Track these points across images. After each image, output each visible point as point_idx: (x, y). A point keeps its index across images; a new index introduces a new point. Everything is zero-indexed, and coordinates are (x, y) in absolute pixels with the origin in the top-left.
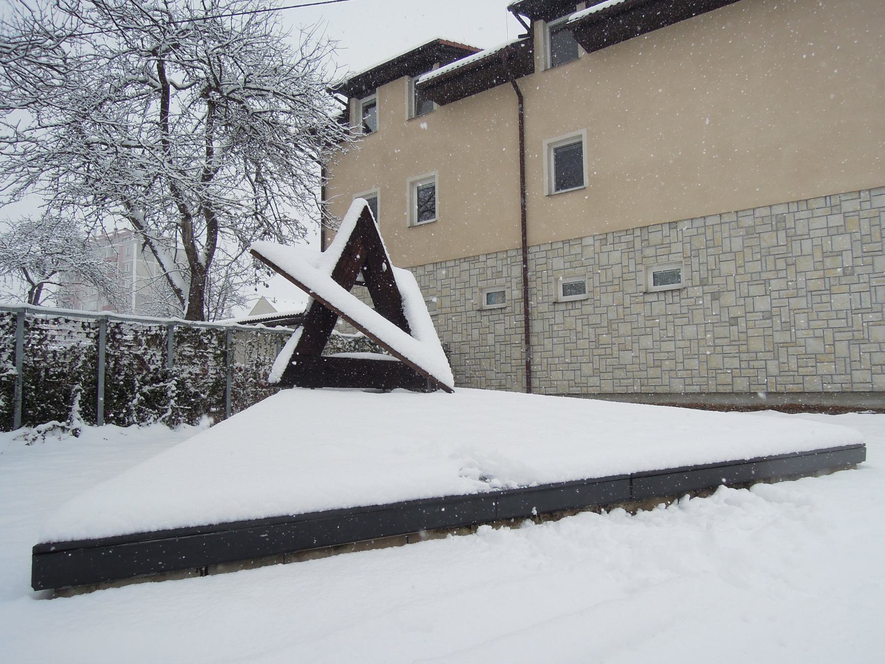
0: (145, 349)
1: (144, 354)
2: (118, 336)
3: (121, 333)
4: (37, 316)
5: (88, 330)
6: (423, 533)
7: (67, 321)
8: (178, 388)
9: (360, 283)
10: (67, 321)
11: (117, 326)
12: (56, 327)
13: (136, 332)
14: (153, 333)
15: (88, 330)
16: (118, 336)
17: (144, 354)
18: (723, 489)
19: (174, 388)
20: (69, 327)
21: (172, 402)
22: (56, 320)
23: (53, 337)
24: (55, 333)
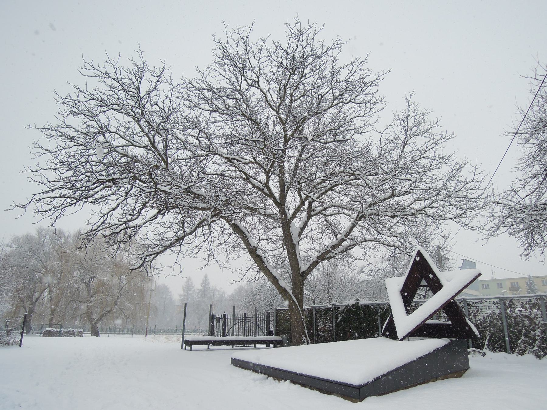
0: (530, 312)
1: (531, 314)
2: (513, 306)
3: (514, 304)
4: (473, 301)
5: (497, 305)
6: (251, 365)
7: (486, 301)
8: (542, 334)
9: (423, 286)
10: (486, 301)
11: (511, 301)
12: (482, 305)
13: (522, 303)
14: (533, 302)
15: (497, 305)
16: (513, 306)
17: (531, 314)
18: (288, 381)
19: (539, 334)
20: (487, 304)
21: (537, 342)
22: (481, 301)
23: (481, 309)
24: (482, 308)
